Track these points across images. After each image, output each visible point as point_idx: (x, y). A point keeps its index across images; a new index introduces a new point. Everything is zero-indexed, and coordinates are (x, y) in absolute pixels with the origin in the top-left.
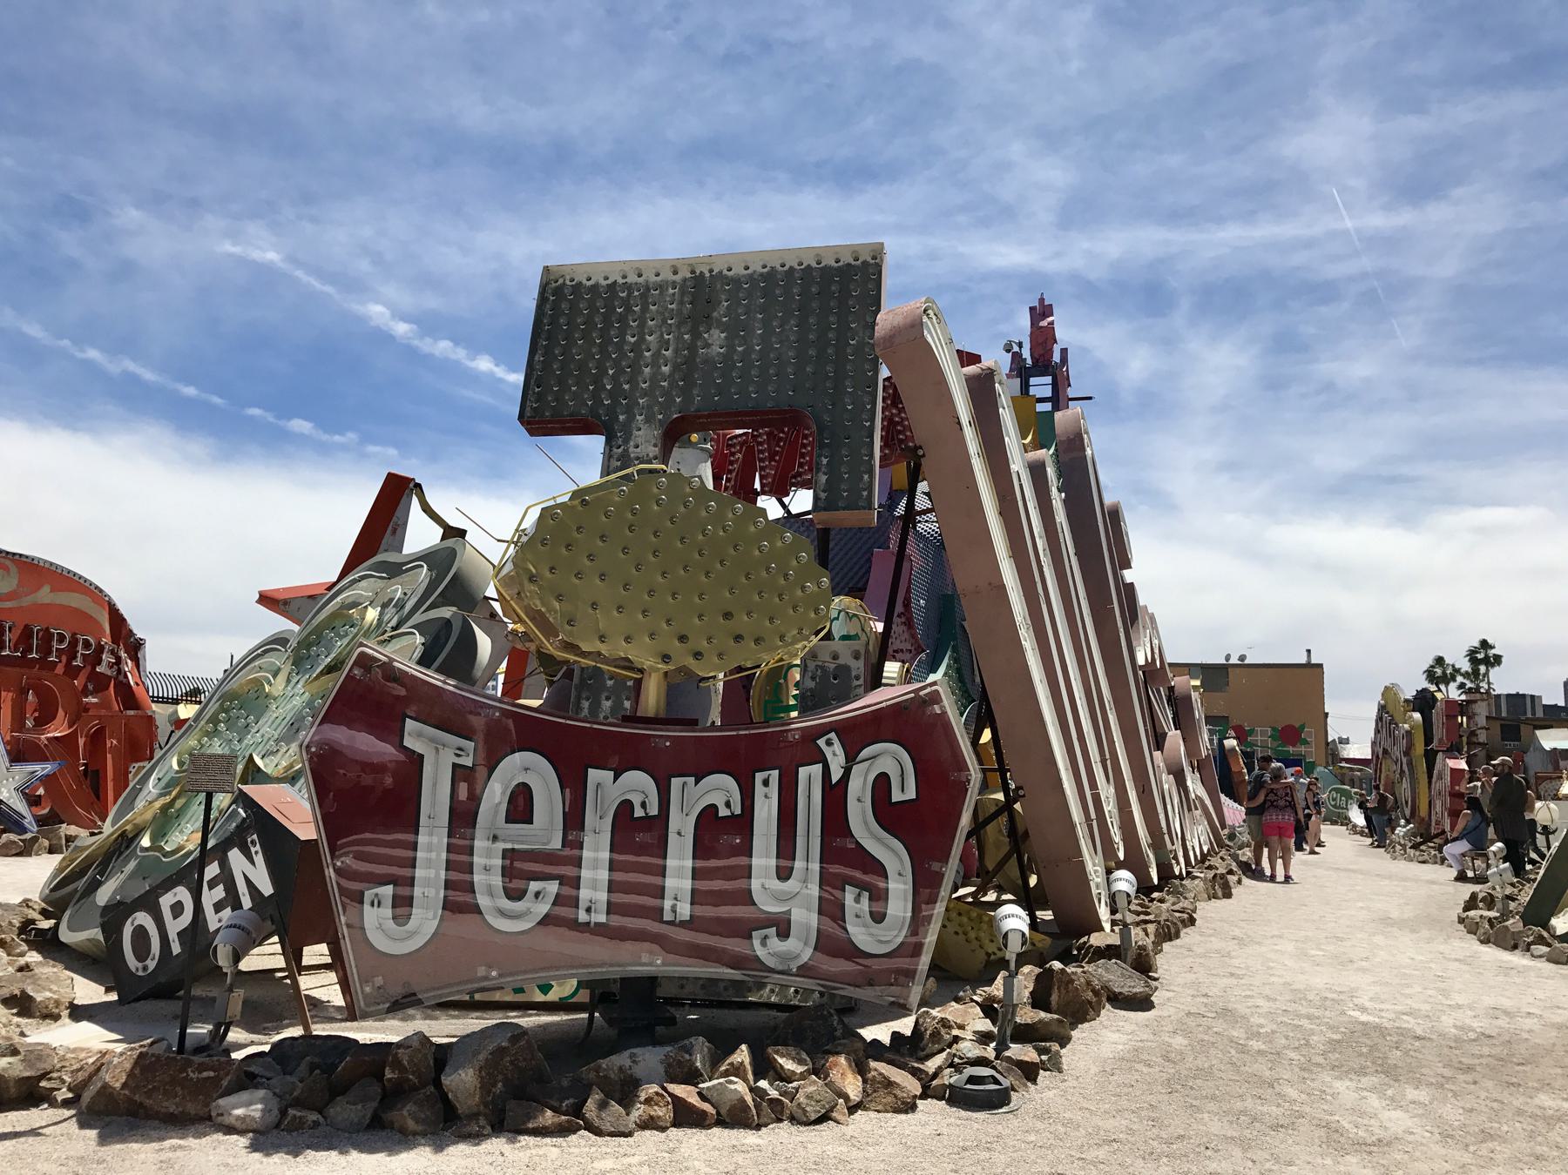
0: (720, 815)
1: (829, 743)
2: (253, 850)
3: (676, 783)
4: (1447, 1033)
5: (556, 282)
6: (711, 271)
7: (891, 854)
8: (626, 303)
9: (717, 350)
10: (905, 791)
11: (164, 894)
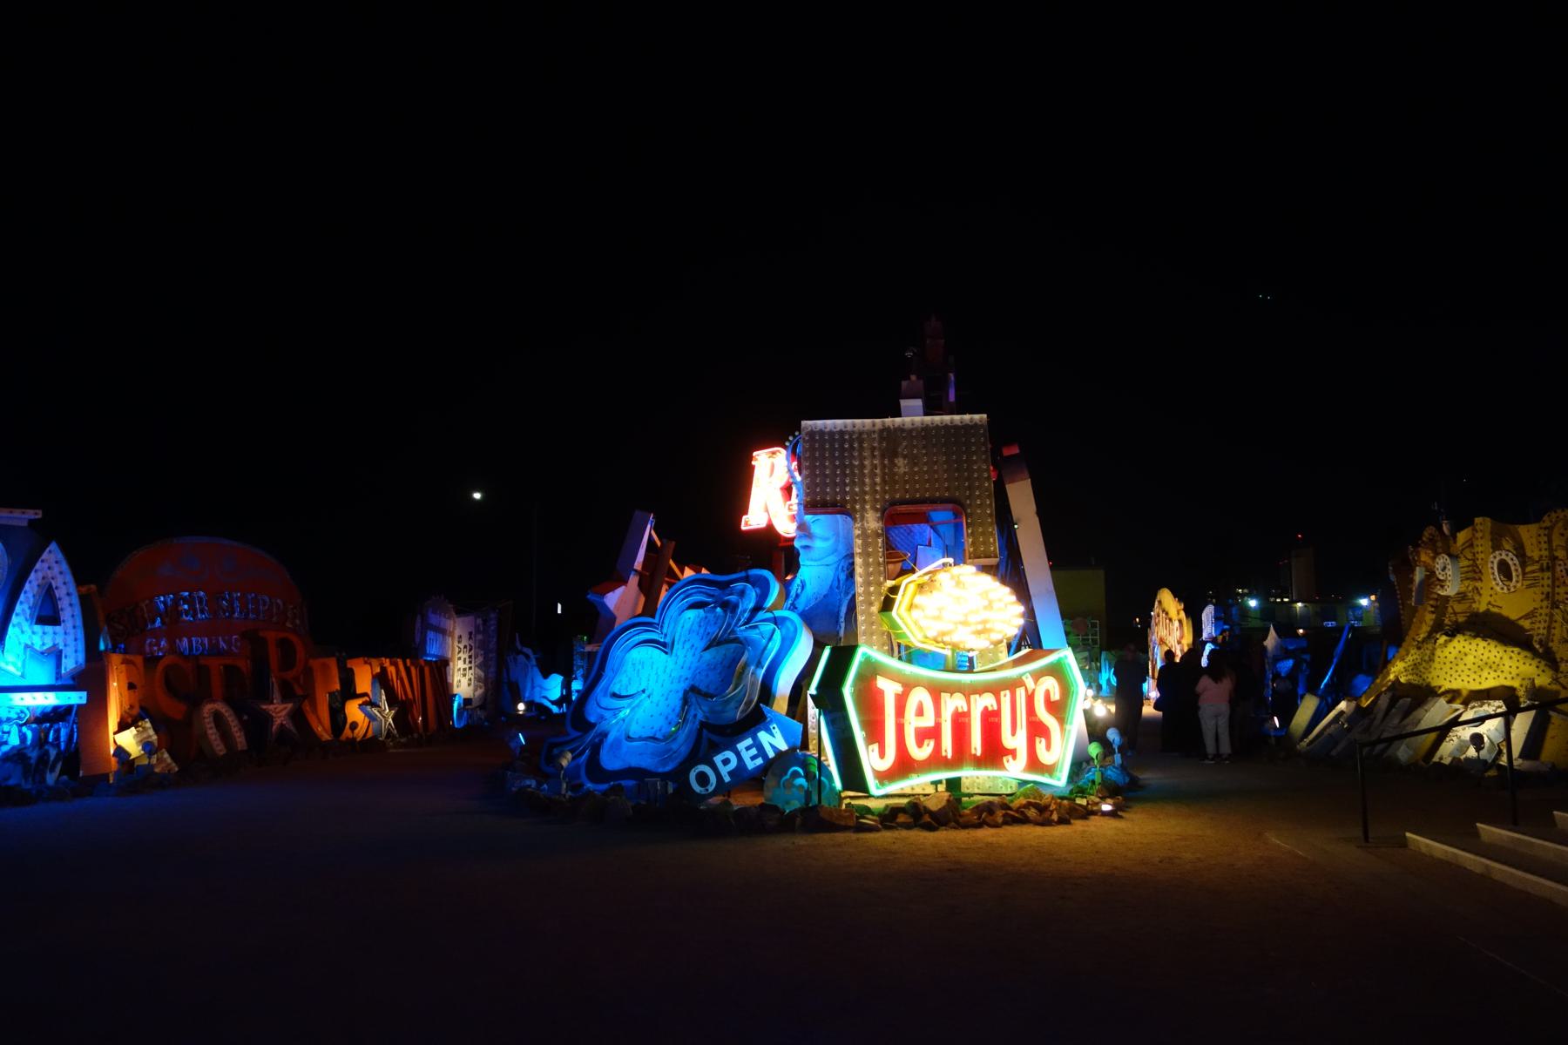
2: (773, 731)
3: (973, 697)
8: (851, 441)
9: (902, 470)
10: (1056, 696)
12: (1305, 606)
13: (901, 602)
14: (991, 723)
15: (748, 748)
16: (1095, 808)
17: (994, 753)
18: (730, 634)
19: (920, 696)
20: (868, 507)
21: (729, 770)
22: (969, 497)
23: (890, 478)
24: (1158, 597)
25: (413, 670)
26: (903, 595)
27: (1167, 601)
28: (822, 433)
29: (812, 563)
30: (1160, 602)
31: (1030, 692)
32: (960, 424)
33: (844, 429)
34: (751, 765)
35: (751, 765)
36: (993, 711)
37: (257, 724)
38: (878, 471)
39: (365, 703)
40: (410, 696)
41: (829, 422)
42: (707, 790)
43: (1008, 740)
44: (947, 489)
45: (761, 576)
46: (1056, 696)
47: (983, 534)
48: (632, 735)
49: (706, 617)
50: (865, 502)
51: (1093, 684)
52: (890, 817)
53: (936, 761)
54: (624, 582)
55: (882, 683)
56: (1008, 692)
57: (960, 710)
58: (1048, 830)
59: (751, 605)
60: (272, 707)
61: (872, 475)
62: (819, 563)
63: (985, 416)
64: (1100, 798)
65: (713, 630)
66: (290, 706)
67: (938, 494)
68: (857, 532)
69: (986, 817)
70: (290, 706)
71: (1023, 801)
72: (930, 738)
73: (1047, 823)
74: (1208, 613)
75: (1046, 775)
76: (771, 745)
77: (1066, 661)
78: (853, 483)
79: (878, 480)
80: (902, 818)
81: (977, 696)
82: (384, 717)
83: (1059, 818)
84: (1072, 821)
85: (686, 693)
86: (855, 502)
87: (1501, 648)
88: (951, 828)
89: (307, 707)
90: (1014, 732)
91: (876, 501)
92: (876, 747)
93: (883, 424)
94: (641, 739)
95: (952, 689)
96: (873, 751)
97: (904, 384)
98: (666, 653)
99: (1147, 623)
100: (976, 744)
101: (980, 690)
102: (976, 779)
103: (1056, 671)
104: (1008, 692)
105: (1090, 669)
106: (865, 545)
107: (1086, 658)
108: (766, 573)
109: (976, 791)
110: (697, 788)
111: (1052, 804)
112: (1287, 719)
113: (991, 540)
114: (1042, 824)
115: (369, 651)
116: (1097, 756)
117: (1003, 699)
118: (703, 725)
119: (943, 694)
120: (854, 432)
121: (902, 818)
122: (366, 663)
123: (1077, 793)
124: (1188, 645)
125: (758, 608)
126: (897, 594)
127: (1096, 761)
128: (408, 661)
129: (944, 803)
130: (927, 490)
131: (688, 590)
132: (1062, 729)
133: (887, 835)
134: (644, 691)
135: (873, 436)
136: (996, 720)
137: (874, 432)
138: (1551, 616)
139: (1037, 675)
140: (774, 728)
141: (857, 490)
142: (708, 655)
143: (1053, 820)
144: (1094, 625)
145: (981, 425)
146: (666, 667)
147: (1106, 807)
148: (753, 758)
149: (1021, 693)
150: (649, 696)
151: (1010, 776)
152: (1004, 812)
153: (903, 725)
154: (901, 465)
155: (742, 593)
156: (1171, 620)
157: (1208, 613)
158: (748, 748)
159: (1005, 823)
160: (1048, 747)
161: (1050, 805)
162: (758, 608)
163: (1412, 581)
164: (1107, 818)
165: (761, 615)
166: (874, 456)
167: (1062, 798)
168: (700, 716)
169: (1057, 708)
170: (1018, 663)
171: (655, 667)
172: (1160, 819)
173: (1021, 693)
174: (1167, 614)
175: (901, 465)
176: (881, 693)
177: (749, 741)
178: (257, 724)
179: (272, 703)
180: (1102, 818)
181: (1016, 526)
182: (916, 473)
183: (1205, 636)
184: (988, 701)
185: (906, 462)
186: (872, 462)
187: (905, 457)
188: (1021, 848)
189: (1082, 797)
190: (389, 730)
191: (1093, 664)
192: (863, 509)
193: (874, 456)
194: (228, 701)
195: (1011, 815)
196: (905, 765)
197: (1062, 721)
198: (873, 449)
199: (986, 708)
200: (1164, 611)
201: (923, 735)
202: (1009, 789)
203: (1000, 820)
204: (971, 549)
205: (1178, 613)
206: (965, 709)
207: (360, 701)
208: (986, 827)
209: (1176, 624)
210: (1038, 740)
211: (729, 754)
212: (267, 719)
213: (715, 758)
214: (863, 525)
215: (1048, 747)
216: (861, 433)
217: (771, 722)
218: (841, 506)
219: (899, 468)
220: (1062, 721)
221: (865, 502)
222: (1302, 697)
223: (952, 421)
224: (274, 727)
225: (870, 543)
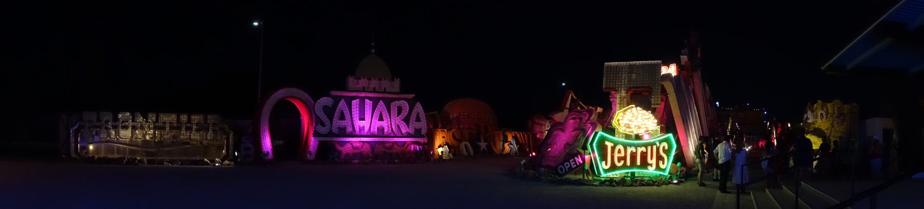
9: (634, 78)
10: (666, 148)
14: (644, 156)
15: (572, 162)
17: (644, 164)
19: (620, 147)
23: (630, 81)
25: (525, 135)
28: (611, 66)
34: (573, 167)
35: (573, 167)
37: (476, 148)
40: (524, 142)
43: (649, 161)
45: (299, 115)
46: (666, 148)
47: (657, 98)
52: (603, 183)
53: (624, 166)
54: (562, 111)
55: (607, 143)
59: (586, 118)
65: (576, 126)
66: (486, 144)
70: (486, 144)
79: (626, 81)
80: (607, 183)
85: (565, 144)
87: (817, 138)
89: (492, 143)
90: (651, 159)
92: (604, 163)
95: (631, 145)
97: (682, 51)
100: (638, 163)
101: (641, 145)
102: (638, 172)
106: (621, 101)
110: (560, 172)
118: (567, 154)
121: (607, 183)
125: (588, 120)
132: (668, 159)
133: (600, 188)
138: (831, 129)
139: (660, 142)
142: (573, 133)
147: (675, 182)
148: (574, 165)
149: (655, 147)
151: (651, 171)
155: (585, 115)
158: (572, 162)
159: (639, 186)
160: (663, 163)
162: (588, 120)
163: (804, 118)
165: (589, 122)
166: (625, 73)
168: (567, 151)
169: (667, 152)
173: (655, 147)
176: (607, 146)
177: (573, 160)
178: (476, 148)
184: (644, 149)
187: (635, 74)
188: (634, 192)
192: (621, 90)
193: (625, 73)
194: (469, 142)
196: (613, 167)
197: (668, 156)
198: (626, 71)
199: (632, 151)
201: (620, 159)
203: (638, 184)
206: (635, 151)
207: (507, 143)
212: (479, 147)
213: (813, 148)
215: (663, 163)
216: (622, 66)
220: (668, 156)
223: (639, 63)
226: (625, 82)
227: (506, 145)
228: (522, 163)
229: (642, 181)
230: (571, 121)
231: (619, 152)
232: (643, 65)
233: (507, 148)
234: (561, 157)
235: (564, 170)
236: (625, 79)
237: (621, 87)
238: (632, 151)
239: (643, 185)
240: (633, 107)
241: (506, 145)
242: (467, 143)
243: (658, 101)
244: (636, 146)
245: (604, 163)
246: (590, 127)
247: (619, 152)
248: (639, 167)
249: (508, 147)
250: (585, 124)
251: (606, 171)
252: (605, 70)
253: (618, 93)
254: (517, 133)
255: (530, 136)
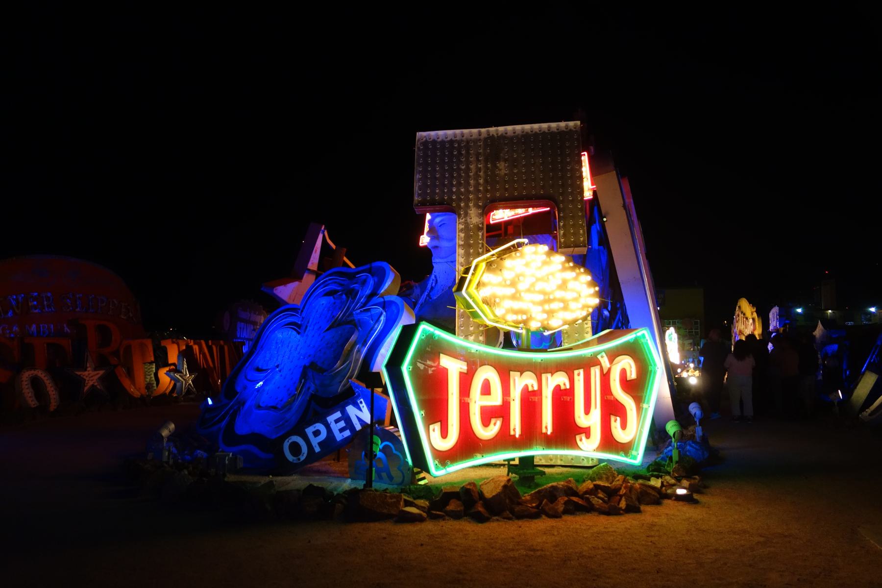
0: (511, 372)
1: (602, 357)
2: (361, 406)
3: (544, 376)
4: (256, 350)
5: (422, 139)
6: (497, 134)
7: (627, 400)
8: (459, 149)
9: (503, 172)
10: (632, 374)
11: (308, 427)
12: (833, 312)
13: (470, 281)
15: (337, 421)
16: (669, 491)
18: (348, 316)
19: (487, 373)
20: (471, 205)
21: (319, 441)
22: (562, 194)
24: (738, 304)
26: (473, 274)
27: (745, 306)
28: (434, 142)
29: (441, 260)
30: (740, 307)
31: (605, 372)
32: (556, 130)
33: (453, 139)
34: (339, 437)
35: (339, 437)
36: (566, 390)
38: (481, 174)
39: (170, 371)
41: (441, 133)
42: (299, 459)
43: (581, 419)
44: (543, 187)
46: (632, 374)
47: (573, 226)
48: (261, 404)
49: (335, 303)
50: (469, 200)
51: (695, 360)
53: (504, 440)
54: (299, 278)
55: (445, 361)
56: (581, 371)
57: (530, 389)
58: (613, 519)
59: (368, 292)
60: (86, 373)
61: (477, 176)
62: (445, 260)
63: (578, 123)
64: (675, 478)
66: (101, 372)
67: (534, 192)
68: (461, 227)
69: (546, 504)
70: (101, 372)
71: (589, 485)
72: (497, 417)
73: (612, 511)
74: (774, 313)
75: (622, 453)
76: (358, 417)
77: (643, 340)
78: (459, 184)
79: (481, 181)
80: (452, 506)
81: (549, 375)
82: (184, 379)
83: (627, 505)
84: (642, 507)
86: (460, 200)
88: (504, 518)
89: (121, 371)
90: (587, 410)
91: (479, 199)
92: (436, 427)
93: (488, 132)
94: (267, 408)
95: (522, 367)
96: (434, 430)
98: (299, 333)
99: (731, 321)
103: (634, 351)
104: (581, 371)
105: (694, 350)
106: (467, 237)
107: (691, 344)
108: (384, 264)
109: (559, 463)
110: (290, 458)
111: (623, 488)
112: (849, 392)
113: (581, 231)
114: (608, 513)
115: (176, 337)
116: (674, 434)
117: (576, 377)
118: (313, 397)
119: (511, 373)
120: (462, 141)
122: (173, 343)
123: (653, 471)
124: (759, 335)
126: (468, 274)
127: (673, 439)
128: (210, 341)
129: (499, 489)
130: (524, 188)
131: (326, 281)
132: (639, 409)
134: (277, 367)
135: (479, 144)
136: (568, 399)
137: (480, 140)
139: (613, 355)
140: (361, 402)
141: (463, 190)
143: (621, 509)
144: (696, 323)
145: (576, 131)
146: (298, 346)
147: (681, 492)
148: (342, 430)
149: (595, 372)
150: (280, 371)
152: (566, 499)
153: (468, 404)
154: (502, 167)
155: (364, 283)
156: (747, 318)
157: (774, 313)
158: (337, 421)
159: (566, 512)
160: (624, 426)
161: (620, 489)
164: (681, 503)
165: (376, 300)
166: (478, 161)
167: (637, 477)
170: (601, 340)
171: (290, 345)
172: (739, 505)
173: (595, 372)
174: (744, 314)
175: (502, 167)
177: (338, 415)
179: (86, 370)
180: (676, 503)
181: (605, 219)
182: (515, 174)
183: (771, 328)
184: (560, 379)
185: (506, 165)
186: (477, 165)
187: (506, 161)
189: (657, 477)
190: (189, 388)
191: (696, 347)
193: (478, 161)
195: (574, 502)
197: (639, 400)
198: (478, 155)
199: (526, 387)
200: (742, 312)
201: (488, 415)
202: (591, 462)
203: (561, 508)
204: (562, 240)
205: (752, 314)
206: (536, 388)
207: (167, 369)
208: (544, 516)
209: (751, 321)
210: (613, 418)
211: (320, 427)
212: (81, 382)
214: (466, 220)
215: (624, 426)
216: (468, 142)
217: (358, 397)
218: (448, 204)
219: (500, 170)
220: (639, 400)
221: (469, 200)
222: (864, 373)
224: (86, 388)
225: (471, 236)
226: (477, 184)
227: (163, 373)
228: (165, 433)
229: (570, 491)
230: (324, 301)
231: (486, 390)
232: (526, 136)
233: (165, 378)
234: (295, 407)
235: (304, 449)
236: (477, 176)
237: (468, 200)
238: (526, 387)
239: (573, 509)
240: (520, 245)
241: (163, 373)
242: (40, 374)
243: (576, 234)
244: (539, 370)
245: (436, 427)
246: (381, 314)
247: (486, 390)
248: (550, 441)
249: (168, 379)
250: (365, 304)
251: (444, 458)
252: (418, 153)
253: (459, 215)
254: (192, 343)
255: (226, 348)
